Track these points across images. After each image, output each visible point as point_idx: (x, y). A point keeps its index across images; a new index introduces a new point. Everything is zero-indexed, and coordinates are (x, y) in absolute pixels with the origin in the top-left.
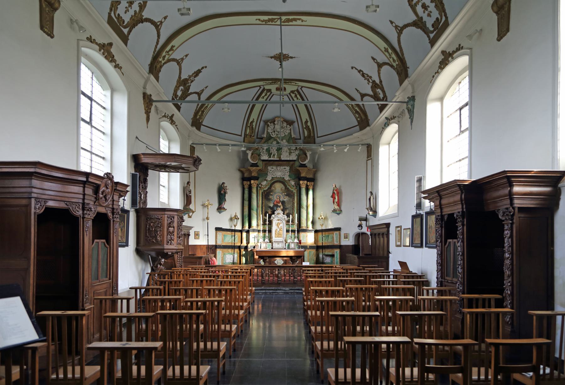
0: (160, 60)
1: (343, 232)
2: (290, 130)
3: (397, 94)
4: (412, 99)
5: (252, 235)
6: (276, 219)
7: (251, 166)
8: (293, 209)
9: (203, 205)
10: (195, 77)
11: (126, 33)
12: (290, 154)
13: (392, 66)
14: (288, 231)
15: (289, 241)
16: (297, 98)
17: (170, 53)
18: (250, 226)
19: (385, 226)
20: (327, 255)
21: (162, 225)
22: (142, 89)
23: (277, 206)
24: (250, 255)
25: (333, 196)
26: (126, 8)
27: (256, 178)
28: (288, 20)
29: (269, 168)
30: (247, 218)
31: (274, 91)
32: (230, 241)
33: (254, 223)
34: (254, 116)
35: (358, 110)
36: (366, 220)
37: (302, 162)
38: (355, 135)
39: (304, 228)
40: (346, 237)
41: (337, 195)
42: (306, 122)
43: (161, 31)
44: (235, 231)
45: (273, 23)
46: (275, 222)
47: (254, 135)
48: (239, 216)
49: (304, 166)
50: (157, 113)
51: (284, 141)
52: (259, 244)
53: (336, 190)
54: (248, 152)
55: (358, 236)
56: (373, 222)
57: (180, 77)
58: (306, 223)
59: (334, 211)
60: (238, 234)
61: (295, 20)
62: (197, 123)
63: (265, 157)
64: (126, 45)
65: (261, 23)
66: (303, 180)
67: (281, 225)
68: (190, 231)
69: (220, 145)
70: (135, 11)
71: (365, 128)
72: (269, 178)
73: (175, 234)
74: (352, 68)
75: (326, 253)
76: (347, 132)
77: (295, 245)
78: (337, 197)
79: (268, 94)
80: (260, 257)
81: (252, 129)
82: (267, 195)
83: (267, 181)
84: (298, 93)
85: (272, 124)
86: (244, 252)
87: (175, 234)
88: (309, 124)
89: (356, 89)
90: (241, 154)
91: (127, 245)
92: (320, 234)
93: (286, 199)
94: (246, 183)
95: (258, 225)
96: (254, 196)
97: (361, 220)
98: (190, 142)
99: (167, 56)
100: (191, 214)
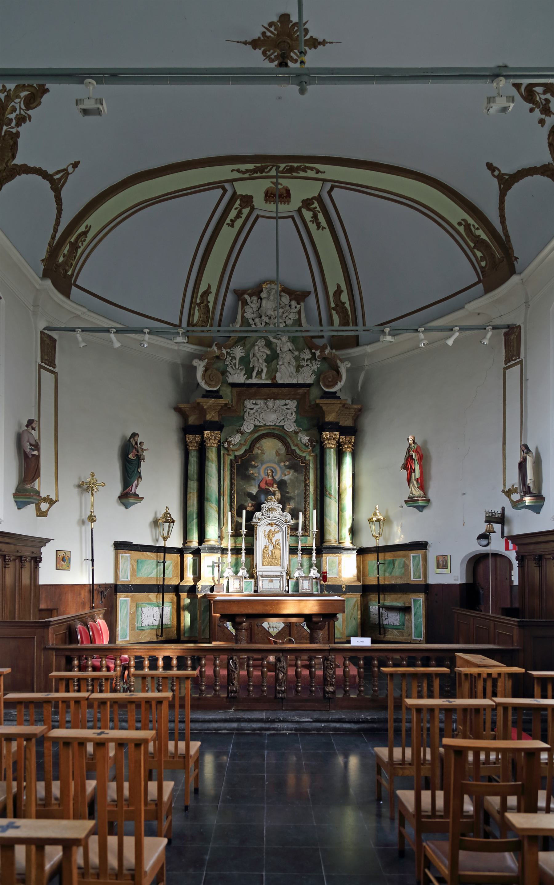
1: (432, 554)
2: (299, 312)
5: (207, 559)
6: (266, 521)
7: (204, 397)
8: (306, 500)
9: (79, 486)
12: (297, 371)
14: (293, 551)
15: (296, 575)
16: (318, 225)
18: (202, 538)
23: (267, 493)
24: (203, 605)
25: (407, 466)
27: (217, 426)
29: (248, 404)
30: (195, 521)
31: (259, 202)
32: (154, 575)
33: (212, 531)
34: (211, 277)
35: (484, 236)
36: (501, 519)
39: (333, 543)
40: (442, 563)
41: (416, 462)
42: (338, 292)
44: (165, 550)
45: (264, 174)
46: (262, 530)
47: (213, 320)
48: (176, 514)
52: (224, 582)
53: (416, 451)
54: (196, 362)
55: (476, 562)
56: (525, 523)
58: (339, 531)
59: (411, 501)
60: (172, 560)
61: (305, 170)
63: (239, 377)
66: (331, 430)
67: (278, 536)
68: (43, 550)
72: (248, 427)
75: (388, 603)
77: (311, 585)
78: (417, 468)
79: (246, 211)
80: (226, 617)
82: (242, 467)
83: (242, 433)
84: (319, 207)
86: (188, 601)
88: (344, 297)
90: (181, 371)
92: (371, 559)
93: (289, 476)
94: (193, 440)
95: (221, 537)
96: (212, 468)
97: (490, 519)
98: (42, 325)
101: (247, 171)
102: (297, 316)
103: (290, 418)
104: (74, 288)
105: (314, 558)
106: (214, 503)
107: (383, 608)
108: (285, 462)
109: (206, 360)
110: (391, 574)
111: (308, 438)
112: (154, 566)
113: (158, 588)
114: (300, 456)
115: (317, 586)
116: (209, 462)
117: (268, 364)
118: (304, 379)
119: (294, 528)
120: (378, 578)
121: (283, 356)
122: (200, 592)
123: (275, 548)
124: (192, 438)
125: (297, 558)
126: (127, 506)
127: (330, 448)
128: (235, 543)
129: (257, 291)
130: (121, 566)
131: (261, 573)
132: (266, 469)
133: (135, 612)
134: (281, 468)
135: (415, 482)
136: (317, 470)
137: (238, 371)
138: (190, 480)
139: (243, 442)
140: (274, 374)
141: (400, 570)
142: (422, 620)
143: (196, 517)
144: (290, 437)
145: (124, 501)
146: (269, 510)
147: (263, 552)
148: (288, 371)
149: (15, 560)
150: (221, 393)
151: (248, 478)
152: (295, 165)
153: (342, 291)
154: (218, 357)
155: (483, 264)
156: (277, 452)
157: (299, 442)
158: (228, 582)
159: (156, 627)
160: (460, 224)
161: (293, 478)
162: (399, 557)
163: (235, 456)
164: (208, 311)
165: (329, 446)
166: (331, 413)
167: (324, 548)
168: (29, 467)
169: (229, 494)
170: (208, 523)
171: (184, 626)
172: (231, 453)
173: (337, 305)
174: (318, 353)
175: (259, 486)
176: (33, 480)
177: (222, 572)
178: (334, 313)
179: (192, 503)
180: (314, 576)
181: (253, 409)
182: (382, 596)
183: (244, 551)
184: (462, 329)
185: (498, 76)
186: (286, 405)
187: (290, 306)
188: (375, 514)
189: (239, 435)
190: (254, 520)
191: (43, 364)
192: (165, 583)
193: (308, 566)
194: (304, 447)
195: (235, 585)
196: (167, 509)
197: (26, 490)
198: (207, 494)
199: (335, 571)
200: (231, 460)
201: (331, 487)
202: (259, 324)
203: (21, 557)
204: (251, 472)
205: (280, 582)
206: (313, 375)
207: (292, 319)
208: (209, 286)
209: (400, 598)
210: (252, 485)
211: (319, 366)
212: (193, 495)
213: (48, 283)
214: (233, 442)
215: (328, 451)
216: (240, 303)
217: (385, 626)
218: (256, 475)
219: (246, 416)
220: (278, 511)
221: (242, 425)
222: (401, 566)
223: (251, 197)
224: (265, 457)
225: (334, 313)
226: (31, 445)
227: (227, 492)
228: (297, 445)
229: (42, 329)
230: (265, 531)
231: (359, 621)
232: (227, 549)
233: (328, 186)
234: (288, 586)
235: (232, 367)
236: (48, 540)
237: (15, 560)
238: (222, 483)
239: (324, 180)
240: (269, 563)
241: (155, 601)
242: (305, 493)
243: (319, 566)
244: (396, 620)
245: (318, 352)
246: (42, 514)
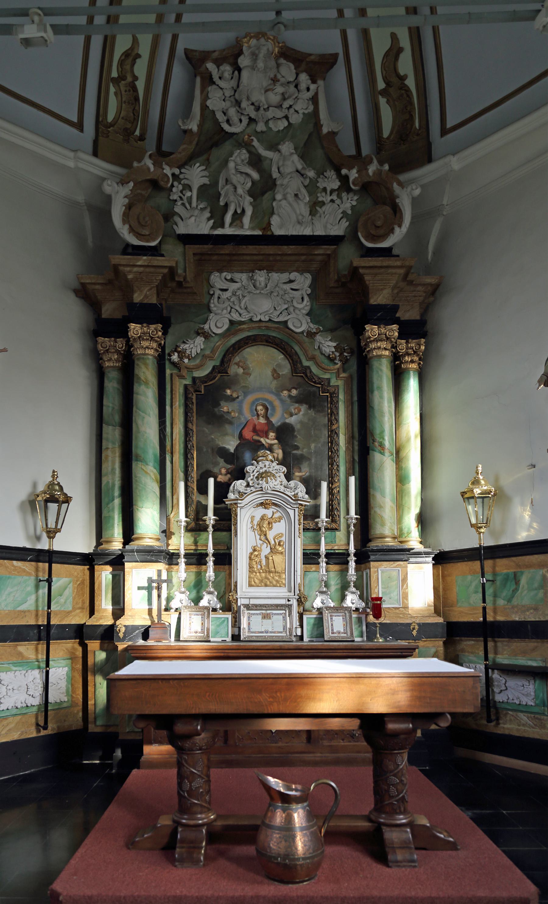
2: (314, 100)
5: (137, 575)
8: (332, 461)
12: (313, 213)
14: (311, 558)
15: (317, 603)
23: (256, 447)
29: (217, 280)
30: (117, 502)
32: (29, 604)
39: (390, 542)
44: (51, 557)
46: (246, 517)
51: (287, 147)
52: (171, 619)
58: (400, 519)
60: (66, 578)
63: (198, 224)
67: (280, 528)
72: (217, 324)
75: (503, 659)
77: (348, 623)
81: (131, 97)
83: (207, 336)
86: (102, 656)
88: (406, 65)
90: (88, 222)
93: (298, 417)
95: (167, 533)
96: (147, 397)
102: (311, 108)
103: (300, 306)
106: (151, 464)
107: (493, 670)
108: (289, 391)
109: (131, 184)
110: (509, 601)
111: (334, 344)
112: (31, 587)
113: (40, 631)
114: (319, 378)
115: (360, 625)
116: (140, 385)
117: (255, 200)
118: (325, 227)
119: (311, 514)
120: (484, 609)
121: (285, 182)
122: (123, 640)
123: (273, 550)
124: (108, 344)
125: (318, 571)
127: (380, 356)
128: (196, 543)
129: (232, 56)
131: (246, 602)
132: (253, 403)
134: (282, 401)
136: (352, 404)
137: (196, 212)
138: (108, 424)
140: (266, 219)
141: (532, 593)
143: (118, 497)
144: (299, 343)
146: (261, 476)
147: (250, 558)
148: (296, 213)
151: (219, 420)
153: (400, 50)
156: (274, 371)
157: (317, 353)
158: (179, 619)
159: (35, 709)
161: (306, 421)
162: (529, 566)
163: (194, 379)
164: (137, 99)
165: (380, 352)
166: (382, 290)
167: (373, 551)
169: (182, 451)
170: (140, 504)
171: (95, 704)
172: (184, 372)
174: (353, 174)
175: (241, 436)
177: (169, 599)
178: (382, 101)
179: (110, 469)
180: (353, 607)
181: (226, 290)
183: (212, 559)
186: (291, 281)
187: (296, 86)
188: (476, 482)
189: (200, 340)
190: (231, 496)
192: (54, 621)
193: (339, 586)
194: (326, 361)
195: (192, 626)
196: (54, 475)
198: (137, 447)
199: (394, 595)
200: (186, 386)
201: (383, 432)
202: (235, 119)
204: (225, 409)
205: (284, 619)
206: (344, 220)
207: (301, 112)
209: (534, 650)
210: (226, 434)
211: (354, 203)
212: (114, 452)
214: (188, 352)
215: (375, 364)
216: (198, 79)
217: (498, 705)
218: (235, 414)
220: (279, 479)
221: (207, 320)
222: (536, 585)
224: (253, 380)
225: (382, 101)
227: (179, 447)
228: (313, 358)
230: (253, 518)
232: (178, 555)
234: (301, 626)
235: (183, 204)
238: (168, 429)
240: (261, 581)
241: (34, 657)
243: (363, 587)
244: (527, 695)
245: (354, 171)
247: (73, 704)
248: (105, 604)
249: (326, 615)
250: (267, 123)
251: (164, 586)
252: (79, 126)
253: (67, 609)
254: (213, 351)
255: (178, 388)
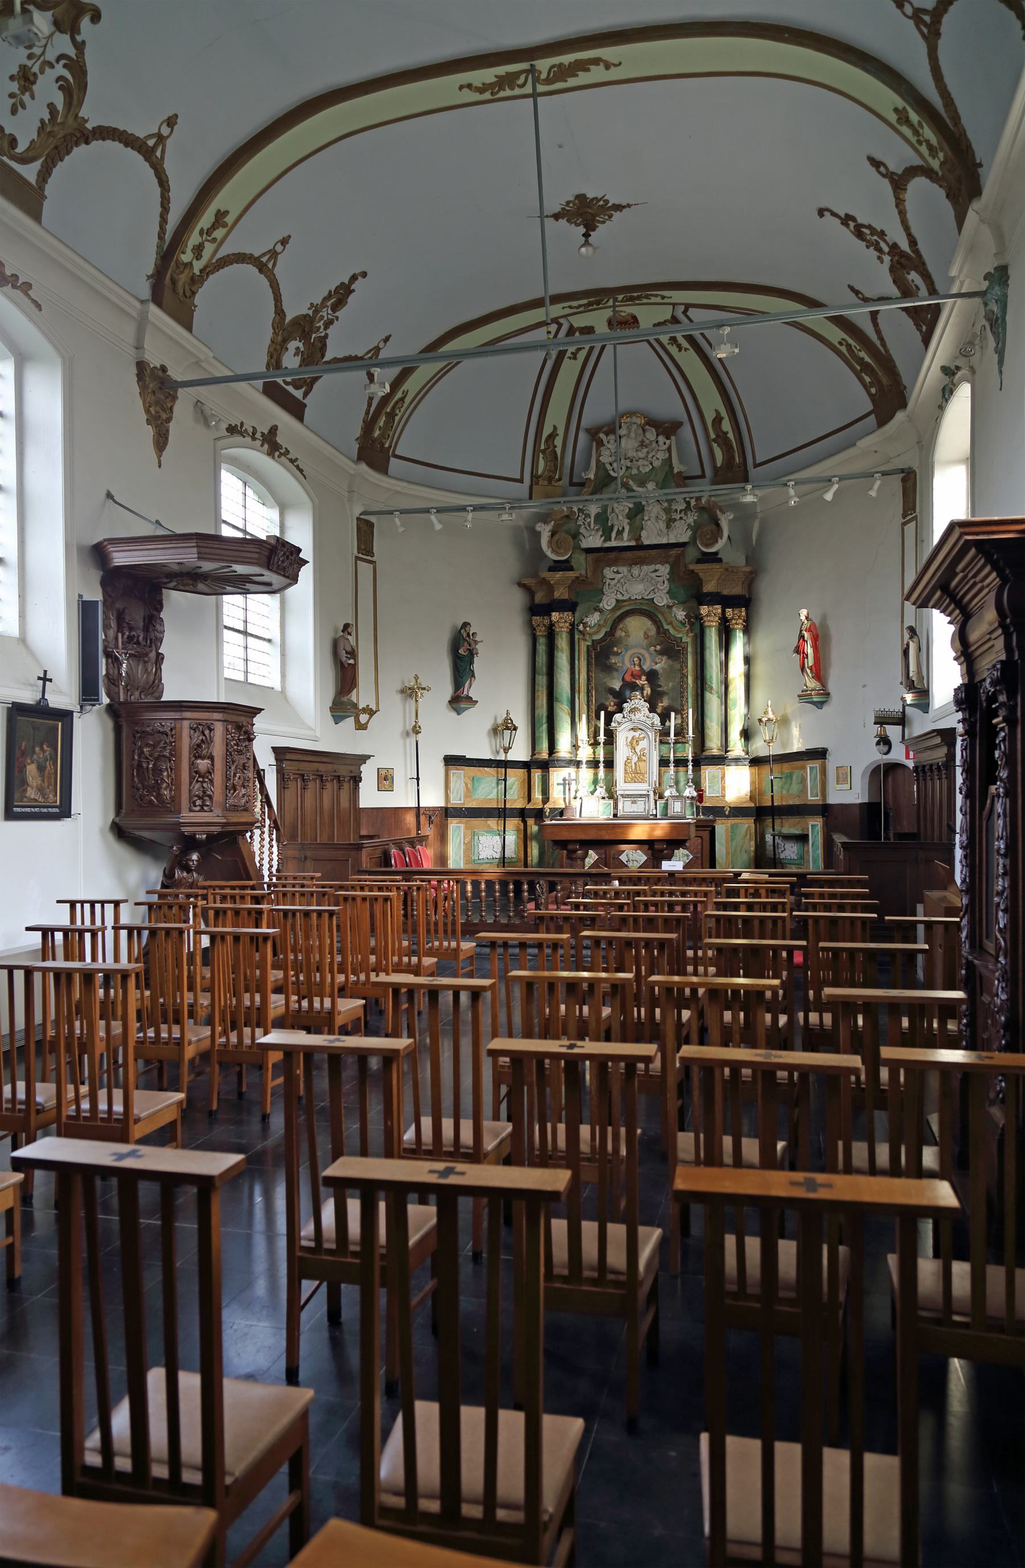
0: (187, 257)
1: (832, 763)
2: (669, 449)
3: (953, 273)
4: (1000, 275)
8: (682, 695)
9: (402, 692)
10: (335, 308)
11: (32, 179)
12: (668, 527)
13: (928, 172)
14: (664, 763)
16: (680, 347)
17: (219, 233)
19: (938, 740)
20: (787, 838)
21: (175, 753)
22: (132, 351)
23: (634, 687)
26: (12, 95)
27: (569, 606)
28: (562, 72)
29: (608, 572)
30: (545, 726)
32: (493, 795)
34: (556, 416)
35: (867, 359)
36: (901, 720)
37: (707, 546)
38: (863, 443)
39: (715, 752)
42: (718, 420)
43: (168, 166)
44: (506, 764)
45: (517, 91)
47: (559, 473)
48: (521, 720)
49: (713, 558)
50: (206, 423)
51: (651, 486)
52: (576, 804)
53: (809, 630)
54: (539, 527)
55: (885, 774)
57: (280, 312)
60: (515, 777)
62: (374, 452)
63: (593, 540)
64: (37, 217)
65: (477, 97)
67: (644, 744)
69: (439, 511)
70: (51, 107)
71: (891, 417)
72: (608, 603)
73: (218, 777)
74: (821, 212)
75: (785, 831)
76: (842, 434)
77: (684, 807)
81: (553, 457)
83: (601, 611)
85: (612, 437)
86: (535, 828)
87: (218, 777)
88: (726, 426)
89: (852, 288)
90: (526, 535)
91: (64, 812)
93: (661, 665)
95: (575, 747)
96: (562, 660)
97: (882, 720)
98: (357, 511)
99: (209, 248)
100: (363, 718)
101: (580, 306)
102: (667, 455)
104: (392, 460)
105: (690, 772)
112: (494, 785)
118: (676, 537)
119: (665, 733)
126: (459, 712)
127: (710, 626)
128: (594, 753)
130: (452, 785)
131: (622, 793)
133: (470, 842)
134: (650, 654)
135: (809, 671)
139: (602, 622)
142: (820, 852)
144: (663, 614)
145: (454, 706)
146: (632, 711)
149: (332, 780)
150: (573, 563)
152: (635, 294)
153: (722, 419)
154: (567, 517)
155: (873, 390)
160: (840, 343)
162: (797, 768)
163: (593, 641)
164: (556, 458)
168: (345, 677)
172: (587, 637)
173: (718, 436)
176: (350, 691)
178: (715, 445)
182: (777, 822)
184: (842, 478)
185: (723, 325)
186: (656, 571)
188: (766, 713)
189: (597, 615)
190: (613, 724)
191: (360, 555)
194: (680, 625)
196: (508, 713)
197: (343, 703)
201: (711, 677)
203: (339, 777)
208: (555, 428)
213: (363, 467)
215: (707, 631)
216: (594, 444)
219: (606, 588)
223: (593, 328)
225: (715, 445)
226: (347, 653)
228: (670, 623)
229: (357, 515)
231: (752, 854)
233: (682, 308)
236: (369, 757)
237: (332, 780)
239: (674, 305)
242: (682, 686)
246: (361, 727)
247: (519, 860)
248: (537, 795)
249: (670, 801)
250: (638, 468)
251: (573, 783)
252: (521, 481)
253: (516, 800)
254: (605, 622)
255: (583, 647)
